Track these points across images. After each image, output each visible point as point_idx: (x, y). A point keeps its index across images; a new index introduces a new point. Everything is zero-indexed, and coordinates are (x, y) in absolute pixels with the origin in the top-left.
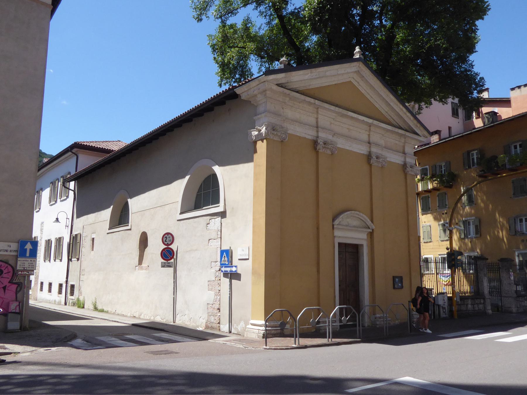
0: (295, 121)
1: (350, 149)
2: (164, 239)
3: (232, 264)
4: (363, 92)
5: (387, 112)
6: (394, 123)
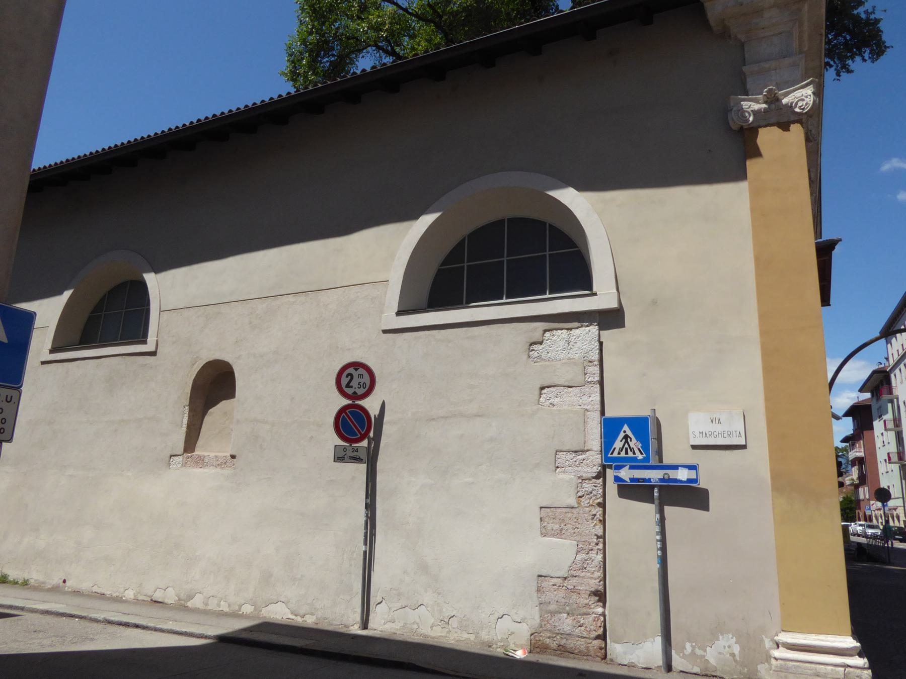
2: (344, 381)
3: (661, 460)
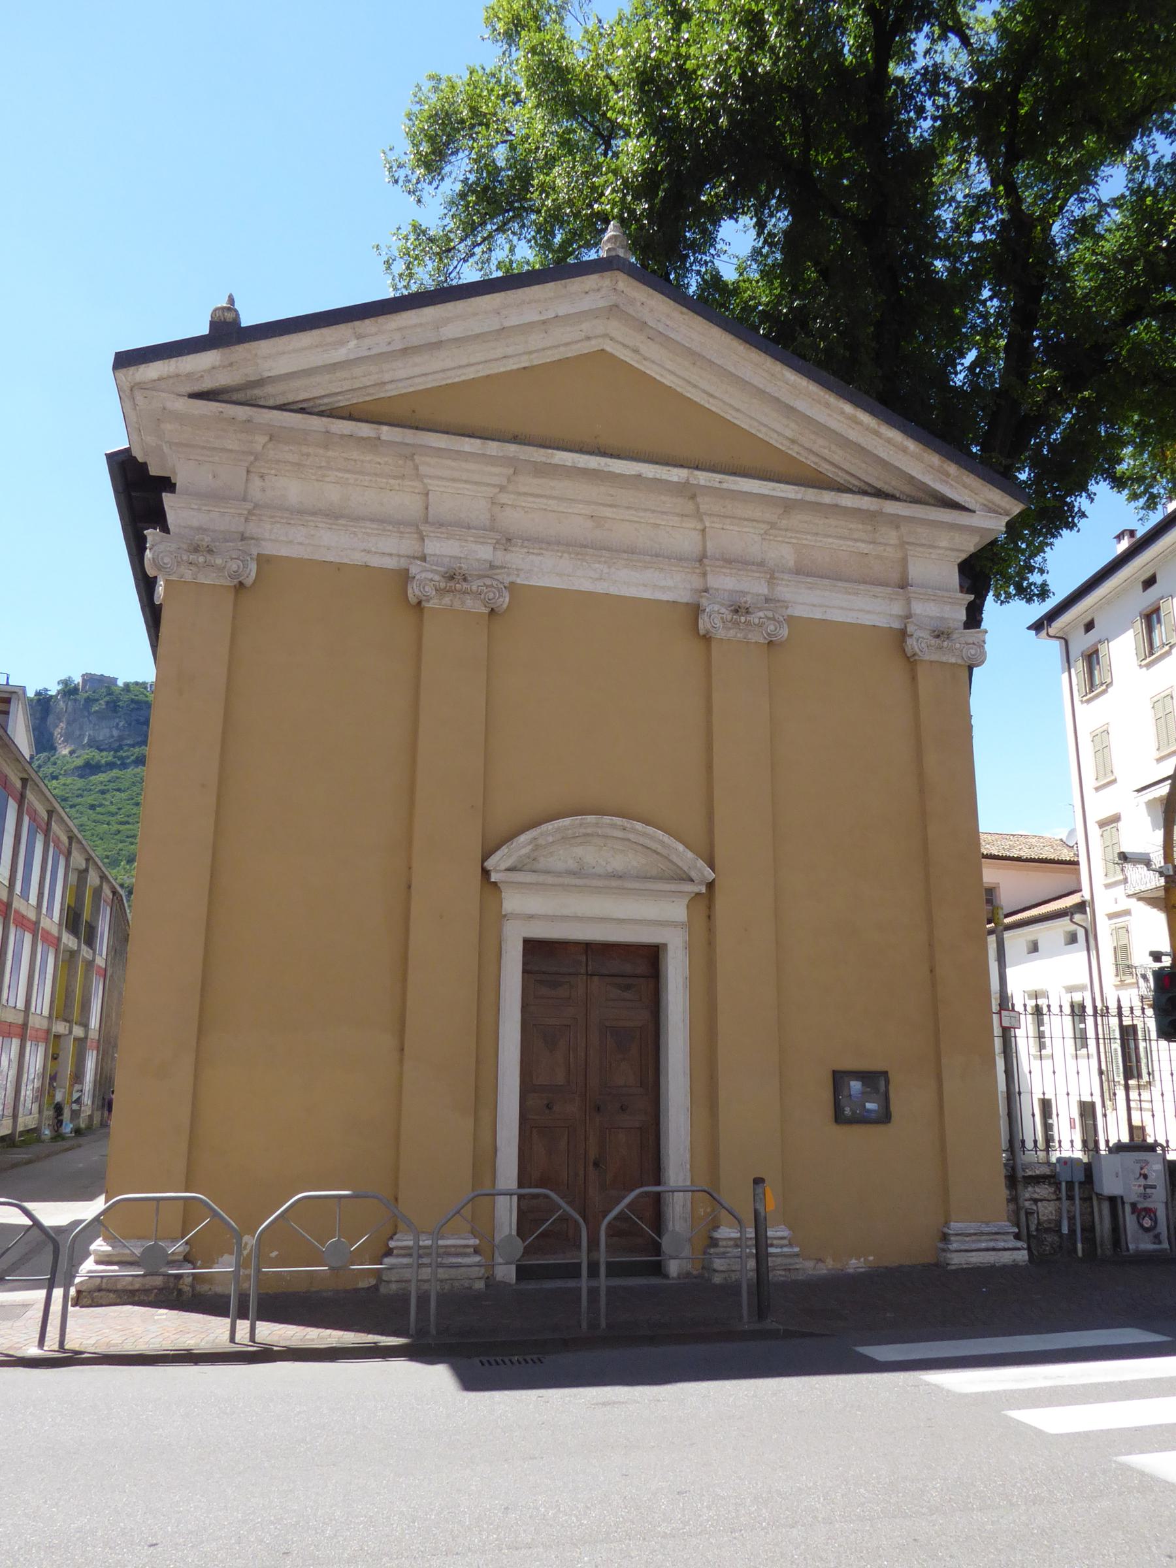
0: (302, 513)
1: (601, 588)
4: (669, 380)
5: (793, 441)
6: (841, 478)
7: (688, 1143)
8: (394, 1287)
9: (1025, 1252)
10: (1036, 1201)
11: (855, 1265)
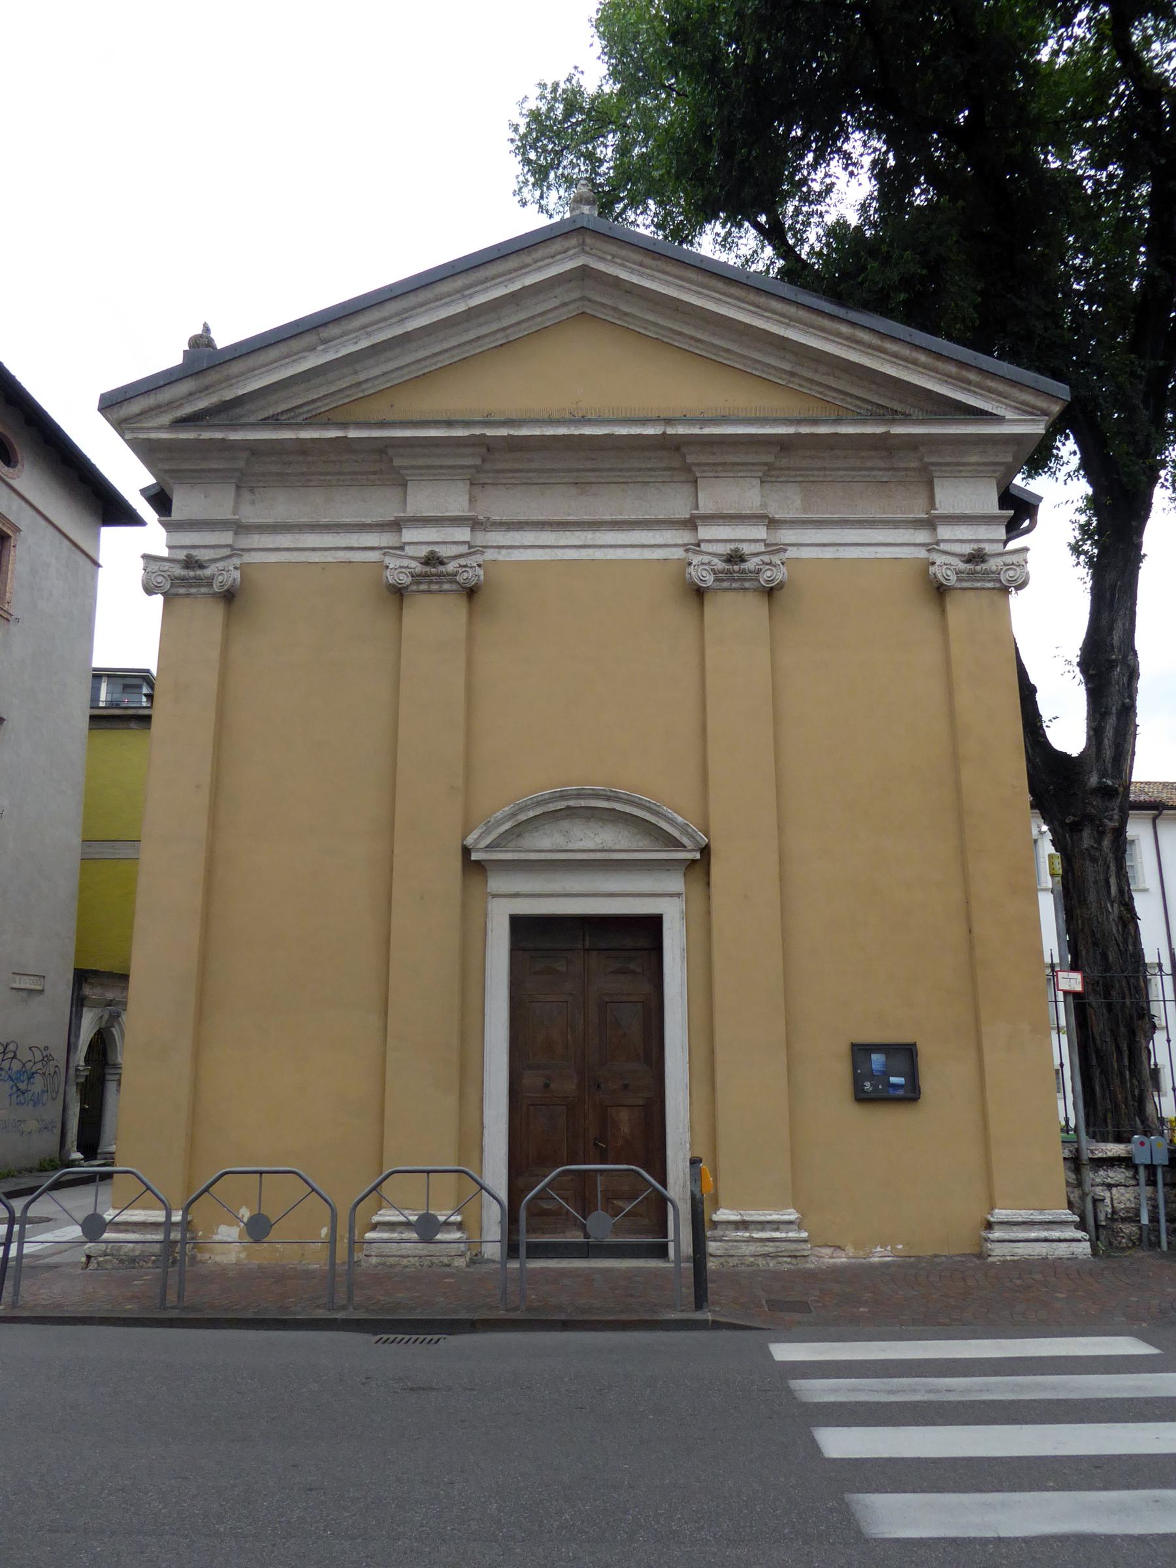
7: (687, 1120)
8: (374, 1260)
9: (1088, 1244)
10: (1109, 1186)
11: (880, 1255)
